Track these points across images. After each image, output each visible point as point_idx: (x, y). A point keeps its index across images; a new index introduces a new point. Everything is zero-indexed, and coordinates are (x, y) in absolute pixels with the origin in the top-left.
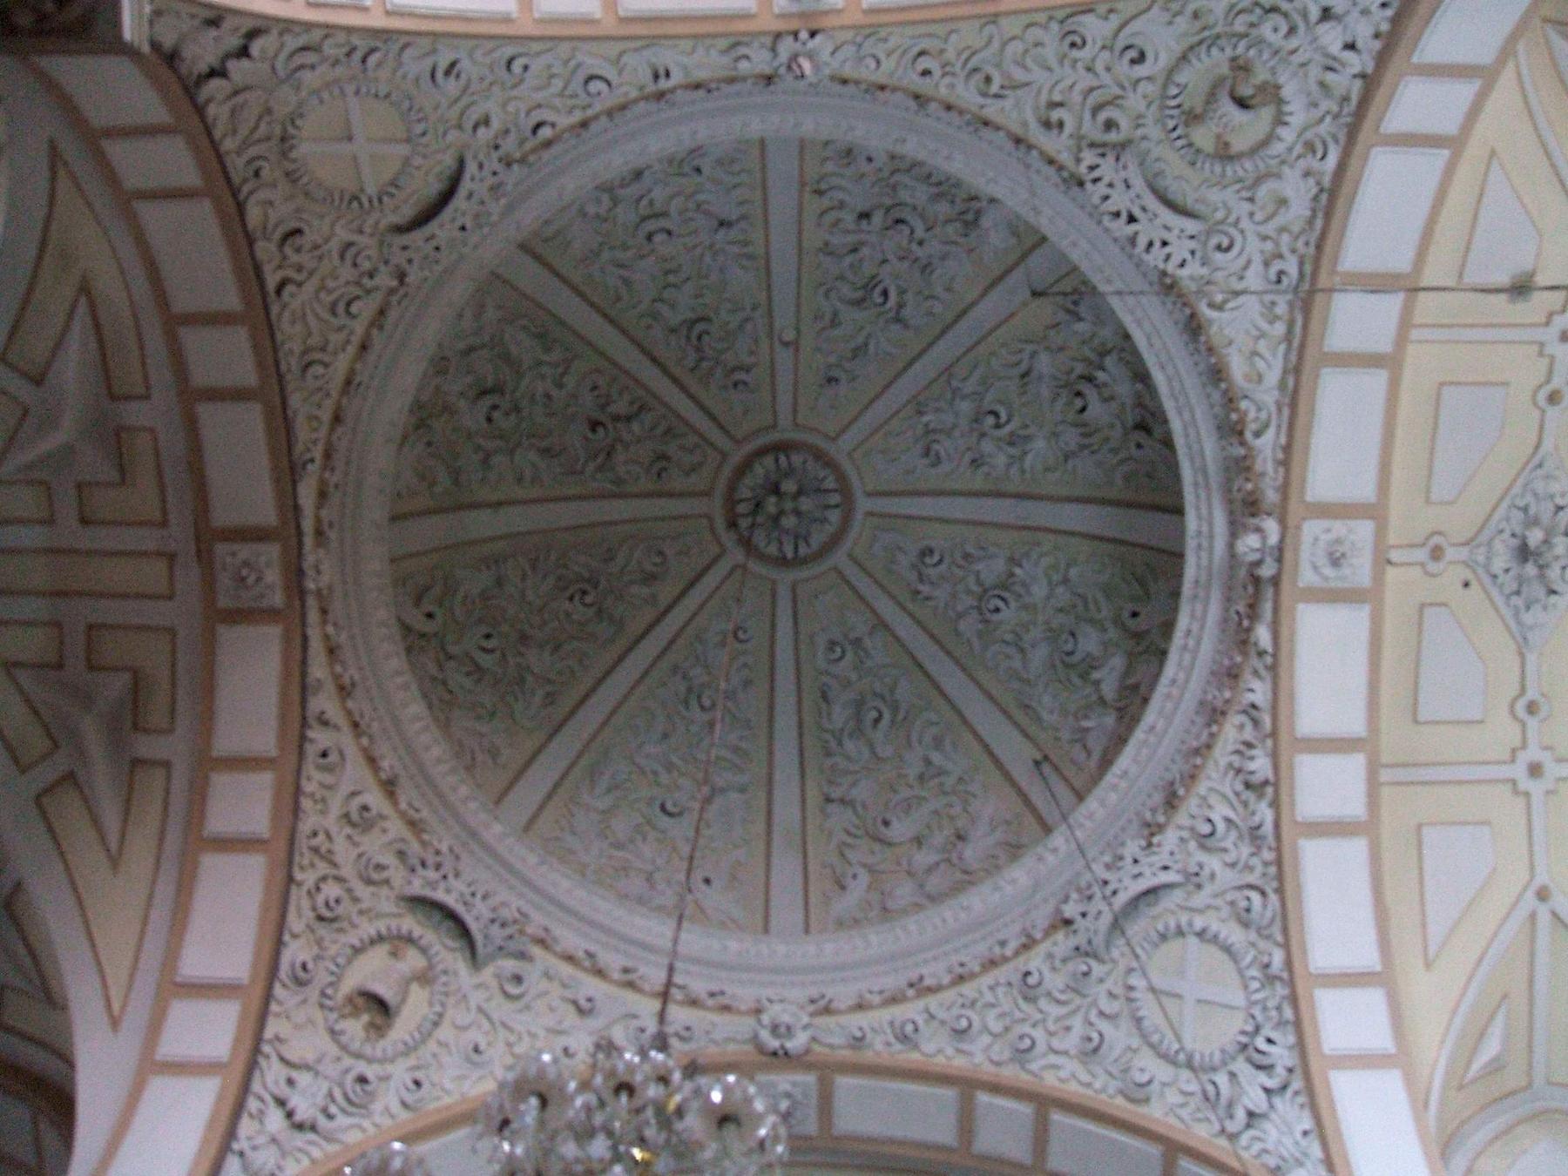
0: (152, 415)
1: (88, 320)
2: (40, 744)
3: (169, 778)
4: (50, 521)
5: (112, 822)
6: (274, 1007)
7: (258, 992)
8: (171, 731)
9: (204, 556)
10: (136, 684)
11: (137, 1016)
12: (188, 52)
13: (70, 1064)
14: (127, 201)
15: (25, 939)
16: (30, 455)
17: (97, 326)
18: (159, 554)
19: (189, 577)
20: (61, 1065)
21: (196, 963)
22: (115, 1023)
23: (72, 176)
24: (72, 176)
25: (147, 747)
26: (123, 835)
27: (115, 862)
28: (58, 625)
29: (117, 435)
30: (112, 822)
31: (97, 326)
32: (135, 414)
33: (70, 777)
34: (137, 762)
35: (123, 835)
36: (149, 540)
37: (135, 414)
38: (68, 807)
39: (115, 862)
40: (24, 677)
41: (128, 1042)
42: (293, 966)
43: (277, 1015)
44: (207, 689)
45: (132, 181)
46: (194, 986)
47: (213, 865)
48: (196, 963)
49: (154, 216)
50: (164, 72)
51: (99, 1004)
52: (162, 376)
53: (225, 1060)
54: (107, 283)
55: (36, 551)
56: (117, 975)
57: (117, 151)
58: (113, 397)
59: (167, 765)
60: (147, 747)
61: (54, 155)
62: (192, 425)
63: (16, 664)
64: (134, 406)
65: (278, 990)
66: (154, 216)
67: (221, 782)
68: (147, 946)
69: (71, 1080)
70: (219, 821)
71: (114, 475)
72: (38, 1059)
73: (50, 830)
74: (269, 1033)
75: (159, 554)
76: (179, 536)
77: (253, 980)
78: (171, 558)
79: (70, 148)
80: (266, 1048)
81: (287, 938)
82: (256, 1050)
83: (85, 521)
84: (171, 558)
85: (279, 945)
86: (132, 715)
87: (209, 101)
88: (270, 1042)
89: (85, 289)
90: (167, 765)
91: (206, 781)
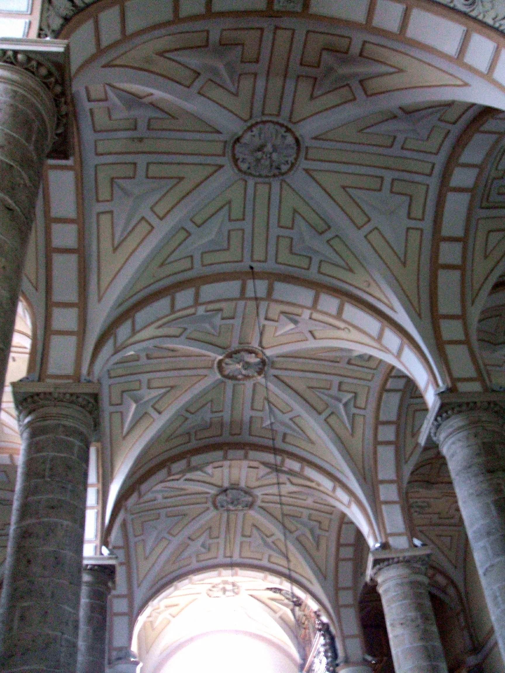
0: (216, 30)
1: (180, 53)
2: (345, 91)
3: (369, 42)
4: (256, 75)
5: (384, 69)
6: (480, 17)
7: (471, 24)
8: (350, 38)
9: (279, 15)
10: (327, 49)
11: (464, 75)
12: (64, 13)
13: (473, 105)
14: (125, 37)
15: (422, 109)
16: (228, 81)
17: (176, 50)
18: (275, 33)
19: (286, 22)
20: (474, 108)
21: (451, 47)
22: (466, 85)
23: (115, 59)
24: (115, 59)
25: (355, 49)
26: (391, 66)
27: (400, 71)
28: (298, 77)
29: (224, 45)
30: (384, 69)
31: (176, 50)
32: (214, 37)
33: (361, 82)
34: (361, 55)
35: (391, 66)
36: (268, 36)
37: (214, 37)
38: (373, 85)
39: (400, 71)
40: (317, 93)
41: (477, 83)
42: (465, 5)
43: (484, 16)
44: (334, 21)
45: (117, 35)
46: (460, 51)
47: (411, 32)
48: (451, 47)
49: (132, 27)
50: (74, 21)
51: (456, 89)
52: (199, 25)
53: (496, 45)
54: (161, 44)
55: (267, 83)
56: (446, 79)
57: (105, 43)
58: (207, 46)
59: (365, 42)
60: (355, 49)
61: (106, 66)
62: (222, 14)
63: (312, 95)
64: (211, 37)
65: (473, 14)
66: (132, 27)
67: (376, 22)
68: (438, 66)
69: (480, 106)
70: (394, 26)
71: (240, 48)
72: (470, 115)
73: (383, 93)
74: (490, 22)
75: (275, 33)
76: (266, 24)
77: (465, 25)
78: (277, 28)
79: (104, 60)
80: (497, 25)
81: (452, 5)
82: (496, 30)
83: (257, 61)
84: (277, 28)
85: (454, 10)
86: (342, 54)
87: (84, 2)
88: (495, 23)
89: (161, 54)
90: (365, 42)
91: (375, 28)
